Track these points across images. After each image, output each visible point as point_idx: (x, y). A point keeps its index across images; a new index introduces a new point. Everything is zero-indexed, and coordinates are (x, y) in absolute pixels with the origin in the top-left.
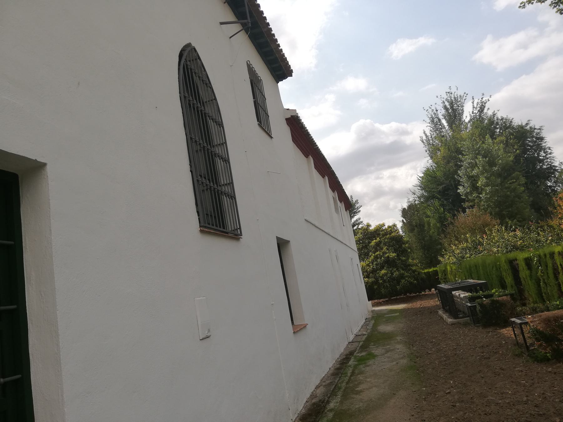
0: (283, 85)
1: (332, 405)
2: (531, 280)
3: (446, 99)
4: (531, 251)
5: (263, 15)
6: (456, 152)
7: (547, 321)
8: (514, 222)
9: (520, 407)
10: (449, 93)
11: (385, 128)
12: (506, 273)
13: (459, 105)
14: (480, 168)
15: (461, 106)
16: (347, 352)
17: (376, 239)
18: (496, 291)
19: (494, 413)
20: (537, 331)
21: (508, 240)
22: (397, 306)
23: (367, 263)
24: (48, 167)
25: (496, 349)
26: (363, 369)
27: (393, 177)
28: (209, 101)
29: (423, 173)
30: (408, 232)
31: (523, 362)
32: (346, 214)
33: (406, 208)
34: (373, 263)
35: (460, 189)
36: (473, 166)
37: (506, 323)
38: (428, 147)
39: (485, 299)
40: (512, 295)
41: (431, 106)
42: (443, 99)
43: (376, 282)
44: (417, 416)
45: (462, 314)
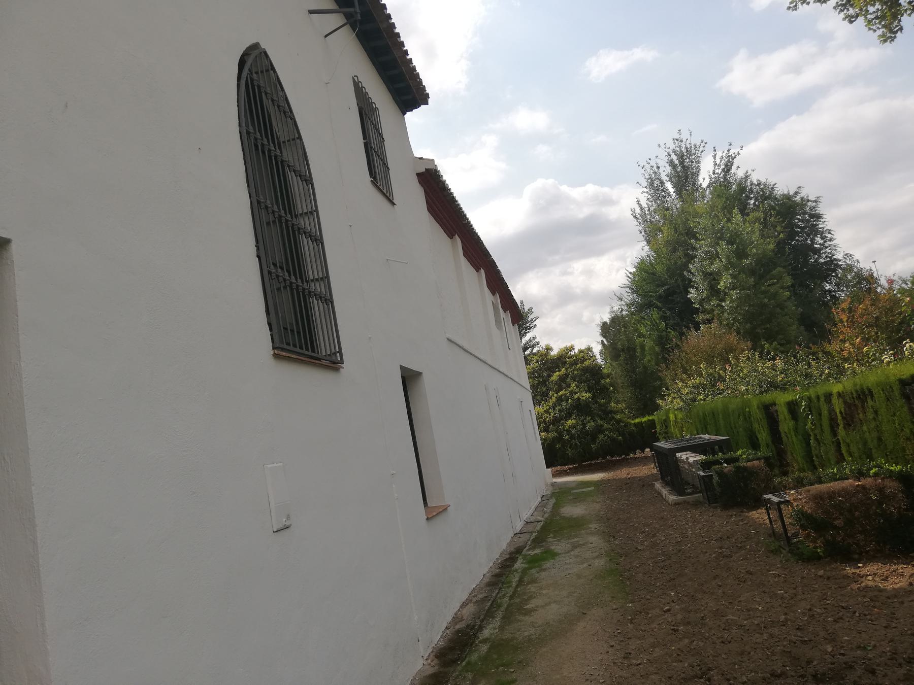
0: (412, 118)
1: (486, 633)
2: (796, 436)
6: (687, 234)
7: (818, 498)
9: (775, 631)
10: (677, 140)
11: (576, 193)
12: (759, 424)
14: (723, 260)
15: (696, 162)
17: (559, 371)
18: (744, 453)
20: (803, 515)
21: (763, 374)
23: (545, 409)
24: (14, 247)
25: (742, 542)
26: (537, 575)
28: (289, 141)
29: (636, 267)
31: (781, 562)
32: (513, 330)
33: (608, 322)
34: (554, 409)
35: (691, 293)
36: (713, 257)
37: (758, 503)
39: (726, 465)
40: (767, 459)
41: (650, 159)
42: (667, 150)
43: (559, 438)
44: (619, 647)
45: (691, 488)
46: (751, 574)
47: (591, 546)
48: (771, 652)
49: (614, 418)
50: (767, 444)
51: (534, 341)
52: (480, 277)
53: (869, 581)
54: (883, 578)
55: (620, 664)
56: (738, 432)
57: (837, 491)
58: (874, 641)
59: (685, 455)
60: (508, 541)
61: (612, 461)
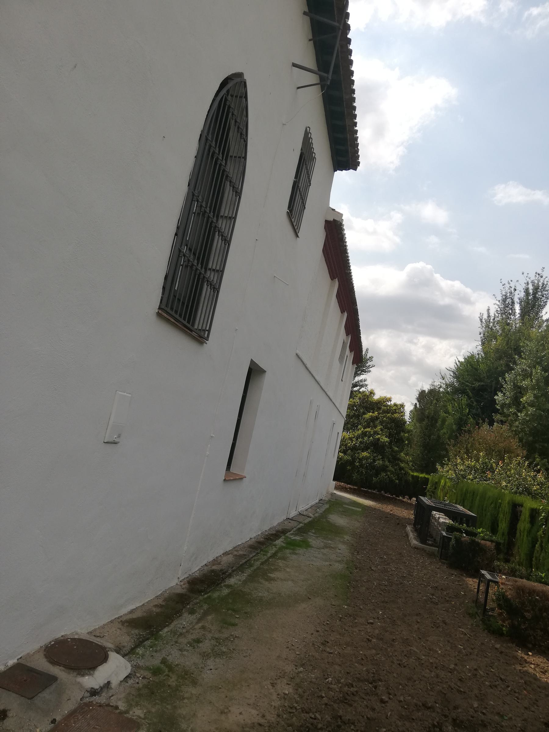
0: (340, 175)
1: (232, 581)
2: (527, 536)
3: (533, 281)
4: (542, 503)
5: (351, 76)
6: (515, 350)
7: (521, 590)
8: (544, 461)
9: (442, 674)
10: (539, 275)
11: (445, 284)
12: (504, 516)
13: (544, 295)
14: (534, 381)
15: (546, 297)
16: (280, 529)
17: (373, 413)
18: (482, 532)
19: (409, 668)
20: (503, 597)
21: (525, 479)
22: (363, 500)
23: (351, 436)
25: (451, 597)
27: (429, 348)
28: (235, 157)
29: (465, 359)
30: (416, 420)
31: (472, 625)
32: (350, 368)
33: (427, 392)
34: (357, 439)
35: (498, 396)
36: (526, 375)
37: (476, 574)
38: (484, 329)
39: (465, 535)
40: (498, 544)
41: (511, 281)
42: (528, 279)
43: (351, 463)
44: (322, 634)
46: (445, 624)
47: (339, 551)
48: (431, 688)
49: (398, 465)
50: (503, 533)
51: (364, 383)
52: (342, 317)
53: (531, 669)
54: (543, 671)
55: (316, 646)
56: (486, 515)
57: (537, 590)
58: (512, 714)
59: (438, 514)
60: (280, 521)
61: (384, 496)
